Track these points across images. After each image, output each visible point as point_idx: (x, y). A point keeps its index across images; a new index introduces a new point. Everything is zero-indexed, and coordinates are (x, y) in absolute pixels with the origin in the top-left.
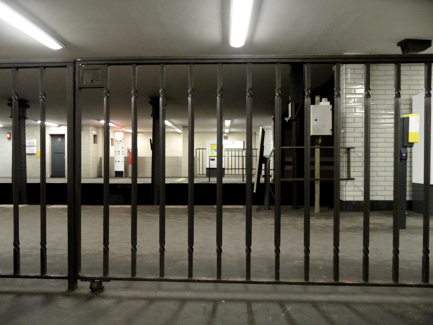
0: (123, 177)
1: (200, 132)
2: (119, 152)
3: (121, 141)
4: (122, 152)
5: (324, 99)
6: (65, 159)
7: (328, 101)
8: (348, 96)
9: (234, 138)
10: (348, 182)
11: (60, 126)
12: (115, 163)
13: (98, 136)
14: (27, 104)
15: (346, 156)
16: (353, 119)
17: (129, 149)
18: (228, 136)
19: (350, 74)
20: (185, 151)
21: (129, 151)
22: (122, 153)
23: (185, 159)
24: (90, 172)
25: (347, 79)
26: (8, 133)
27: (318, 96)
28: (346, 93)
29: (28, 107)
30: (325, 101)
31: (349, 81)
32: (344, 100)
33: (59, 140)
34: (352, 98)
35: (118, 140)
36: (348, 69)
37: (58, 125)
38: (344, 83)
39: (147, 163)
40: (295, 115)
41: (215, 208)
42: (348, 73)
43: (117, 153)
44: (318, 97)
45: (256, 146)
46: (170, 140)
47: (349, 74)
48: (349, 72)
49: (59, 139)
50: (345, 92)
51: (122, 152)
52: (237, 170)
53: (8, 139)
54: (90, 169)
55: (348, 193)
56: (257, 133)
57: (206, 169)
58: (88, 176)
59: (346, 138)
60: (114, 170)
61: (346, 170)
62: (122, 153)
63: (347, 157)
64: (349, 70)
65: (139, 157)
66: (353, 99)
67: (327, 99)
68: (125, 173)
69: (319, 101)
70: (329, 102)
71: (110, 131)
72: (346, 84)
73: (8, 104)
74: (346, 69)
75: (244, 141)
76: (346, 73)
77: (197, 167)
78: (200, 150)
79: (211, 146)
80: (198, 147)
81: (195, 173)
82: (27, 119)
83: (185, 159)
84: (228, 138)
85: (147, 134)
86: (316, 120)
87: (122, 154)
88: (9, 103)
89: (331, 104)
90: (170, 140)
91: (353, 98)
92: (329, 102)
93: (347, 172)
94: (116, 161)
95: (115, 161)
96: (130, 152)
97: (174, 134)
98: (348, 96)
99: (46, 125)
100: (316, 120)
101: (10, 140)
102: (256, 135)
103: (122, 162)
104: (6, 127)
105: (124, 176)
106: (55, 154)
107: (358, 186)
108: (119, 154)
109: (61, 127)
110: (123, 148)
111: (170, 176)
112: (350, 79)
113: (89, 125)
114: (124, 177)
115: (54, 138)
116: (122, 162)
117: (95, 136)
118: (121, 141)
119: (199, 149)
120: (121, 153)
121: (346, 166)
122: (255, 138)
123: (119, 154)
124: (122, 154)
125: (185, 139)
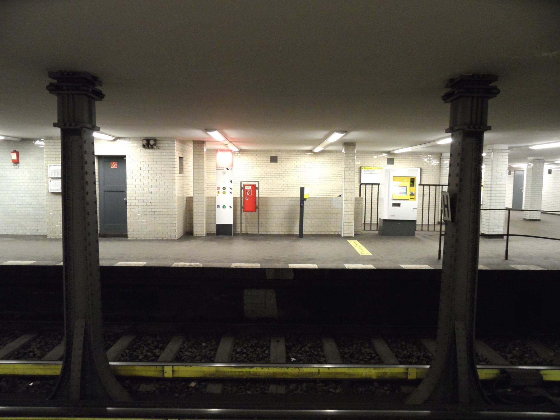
2: (224, 188)
3: (228, 169)
4: (231, 189)
6: (126, 203)
9: (404, 162)
11: (117, 139)
12: (217, 209)
13: (184, 159)
14: (98, 88)
18: (395, 159)
21: (242, 187)
22: (231, 191)
23: (349, 205)
24: (176, 228)
26: (13, 152)
29: (100, 96)
33: (114, 167)
35: (223, 168)
37: (113, 138)
43: (221, 190)
45: (440, 176)
49: (114, 165)
51: (231, 189)
53: (13, 163)
54: (174, 222)
56: (443, 155)
58: (172, 236)
62: (231, 191)
71: (484, 154)
73: (48, 88)
75: (421, 168)
77: (362, 216)
78: (443, 187)
80: (254, 178)
82: (489, 128)
83: (349, 205)
84: (395, 161)
85: (256, 153)
87: (231, 193)
88: (51, 85)
94: (219, 207)
95: (216, 206)
96: (245, 190)
97: (298, 153)
99: (95, 138)
101: (16, 165)
102: (441, 157)
103: (231, 207)
104: (10, 140)
106: (106, 193)
108: (224, 193)
109: (119, 141)
110: (231, 181)
111: (263, 231)
113: (172, 139)
115: (104, 162)
116: (231, 207)
117: (180, 158)
118: (228, 169)
120: (228, 190)
123: (224, 193)
124: (231, 193)
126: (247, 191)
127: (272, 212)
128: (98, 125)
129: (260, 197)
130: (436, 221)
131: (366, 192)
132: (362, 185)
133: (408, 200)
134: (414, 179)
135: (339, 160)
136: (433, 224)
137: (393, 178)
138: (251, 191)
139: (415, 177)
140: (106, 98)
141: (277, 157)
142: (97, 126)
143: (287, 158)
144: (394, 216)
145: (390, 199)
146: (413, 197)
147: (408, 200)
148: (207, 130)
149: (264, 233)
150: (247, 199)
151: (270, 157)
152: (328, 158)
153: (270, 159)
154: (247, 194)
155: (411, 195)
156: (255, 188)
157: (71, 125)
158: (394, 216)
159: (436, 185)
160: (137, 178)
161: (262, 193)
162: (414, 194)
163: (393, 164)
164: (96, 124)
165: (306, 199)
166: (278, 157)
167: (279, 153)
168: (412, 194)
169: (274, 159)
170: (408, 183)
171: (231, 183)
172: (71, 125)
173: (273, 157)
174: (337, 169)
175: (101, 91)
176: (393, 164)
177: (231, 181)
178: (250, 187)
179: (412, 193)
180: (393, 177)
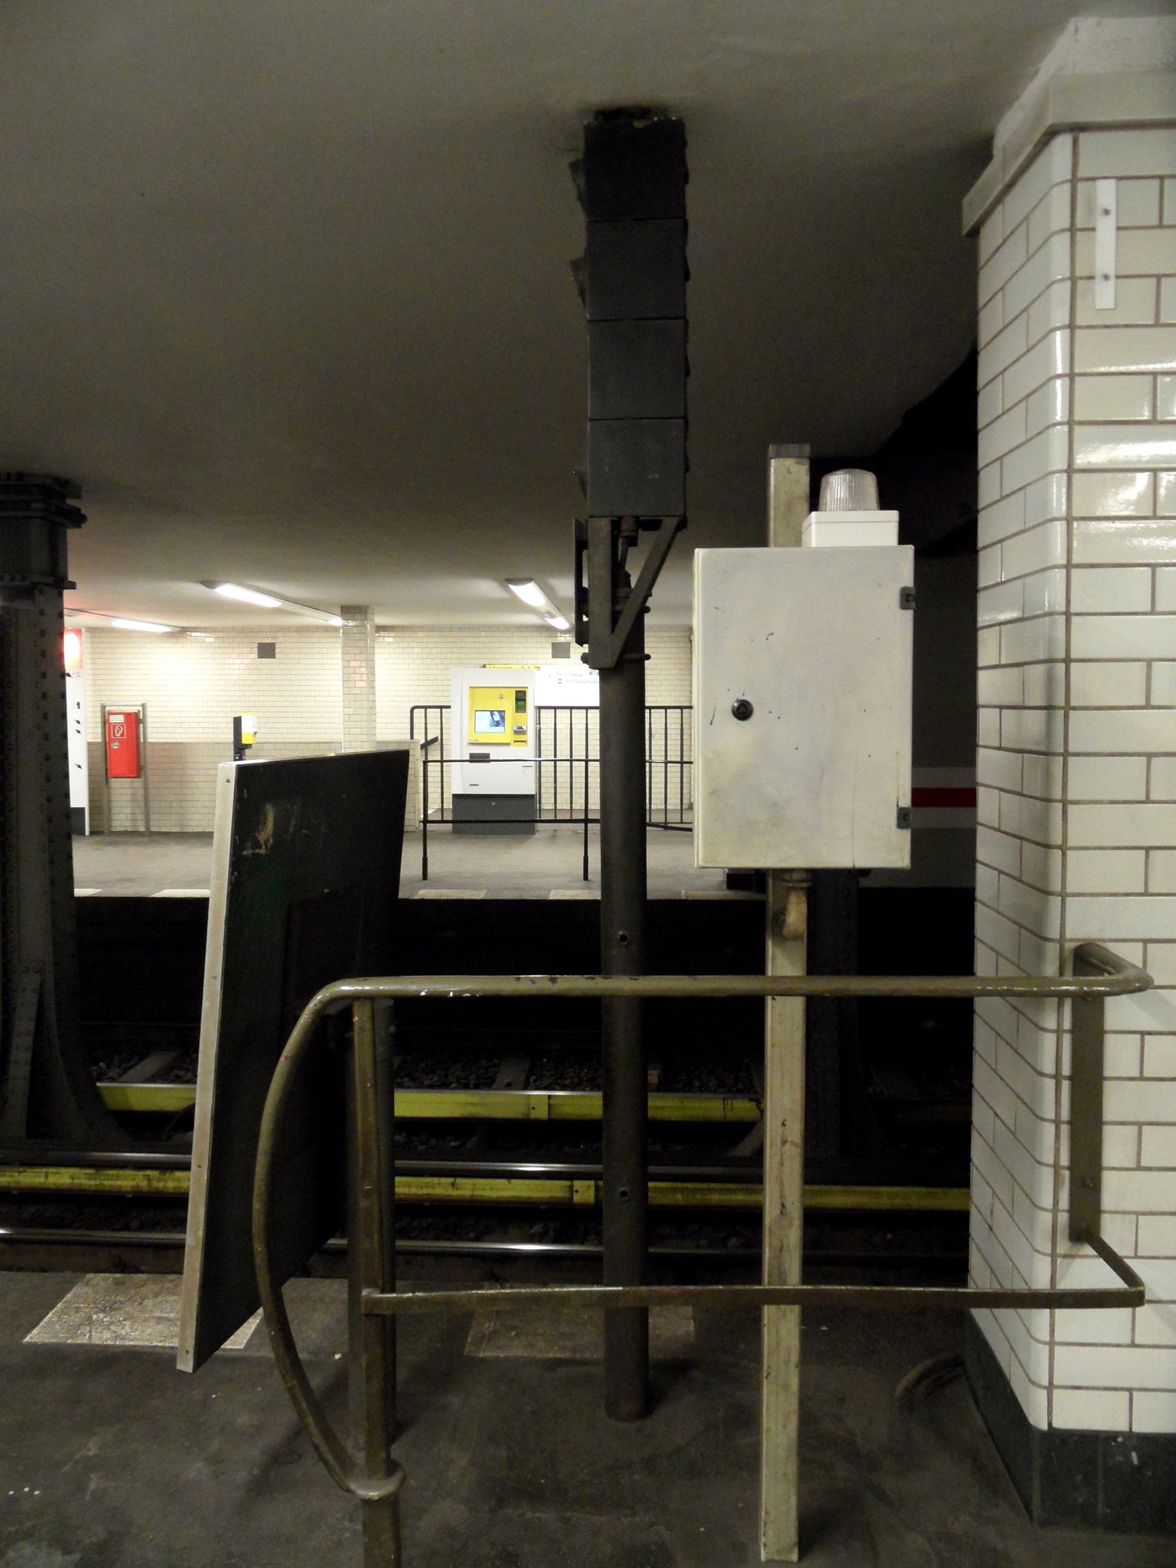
0: (83, 833)
1: (451, 628)
4: (78, 722)
5: (837, 484)
7: (884, 504)
8: (1093, 455)
10: (1078, 1262)
14: (71, 502)
15: (1067, 1024)
16: (1139, 669)
17: (107, 709)
19: (1118, 229)
20: (353, 718)
25: (1081, 284)
27: (792, 447)
28: (1071, 423)
29: (78, 519)
30: (855, 502)
31: (1104, 295)
32: (1057, 487)
34: (1130, 469)
36: (1101, 184)
38: (1061, 316)
39: (192, 772)
40: (613, 630)
41: (1078, 525)
42: (1099, 228)
44: (789, 463)
46: (321, 661)
47: (1106, 229)
48: (1107, 212)
50: (1060, 414)
51: (78, 722)
52: (673, 760)
55: (1070, 1365)
57: (451, 796)
59: (1064, 855)
60: (894, 547)
61: (1057, 1150)
62: (78, 727)
63: (1071, 1078)
64: (1106, 193)
65: (153, 744)
66: (1143, 479)
67: (869, 482)
68: (91, 814)
69: (805, 506)
70: (893, 515)
72: (1072, 327)
74: (1074, 181)
76: (1080, 223)
79: (473, 699)
81: (407, 816)
86: (743, 711)
87: (79, 732)
89: (903, 539)
90: (321, 661)
91: (1067, 996)
92: (893, 515)
93: (1066, 1174)
98: (1093, 455)
100: (743, 711)
103: (79, 767)
105: (91, 826)
107: (1165, 1297)
110: (78, 704)
112: (1112, 282)
114: (87, 833)
116: (79, 767)
119: (426, 708)
121: (1065, 1114)
122: (688, 650)
124: (79, 732)
125: (352, 664)
126: (114, 727)
127: (196, 779)
128: (71, 578)
129: (149, 743)
130: (685, 801)
131: (426, 724)
132: (415, 710)
133: (508, 744)
134: (525, 692)
135: (427, 651)
136: (679, 807)
137: (343, 696)
138: (123, 726)
139: (527, 688)
140: (90, 521)
141: (274, 644)
142: (69, 579)
143: (299, 645)
144: (477, 785)
145: (465, 743)
146: (522, 737)
147: (508, 744)
148: (210, 584)
149: (178, 831)
150: (115, 746)
151: (256, 645)
152: (402, 645)
153: (256, 650)
154: (114, 736)
155: (516, 732)
156: (135, 721)
157: (13, 579)
158: (477, 785)
159: (681, 708)
160: (357, 682)
161: (155, 733)
162: (525, 729)
163: (569, 657)
164: (66, 573)
165: (248, 746)
166: (277, 646)
167: (278, 634)
168: (520, 731)
169: (267, 651)
170: (509, 704)
171: (79, 708)
172: (13, 579)
173: (264, 644)
174: (425, 672)
175: (79, 509)
176: (569, 657)
177: (78, 704)
178: (121, 719)
179: (521, 728)
180: (471, 687)
